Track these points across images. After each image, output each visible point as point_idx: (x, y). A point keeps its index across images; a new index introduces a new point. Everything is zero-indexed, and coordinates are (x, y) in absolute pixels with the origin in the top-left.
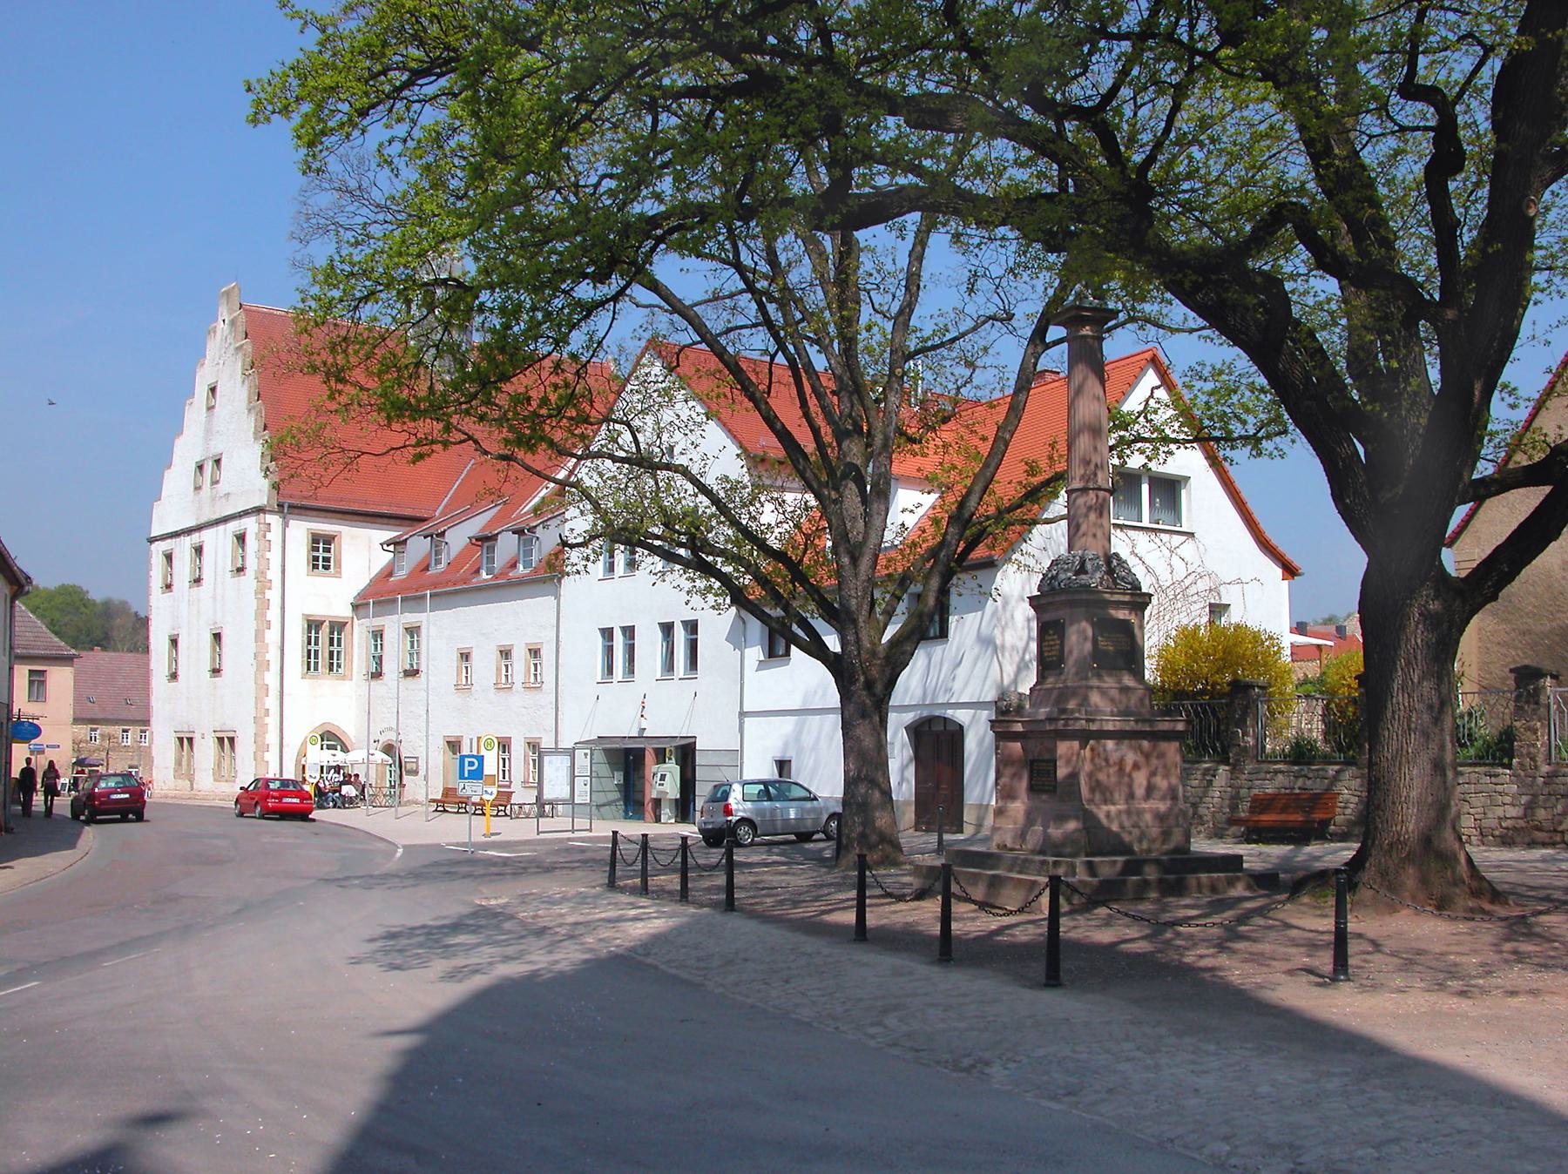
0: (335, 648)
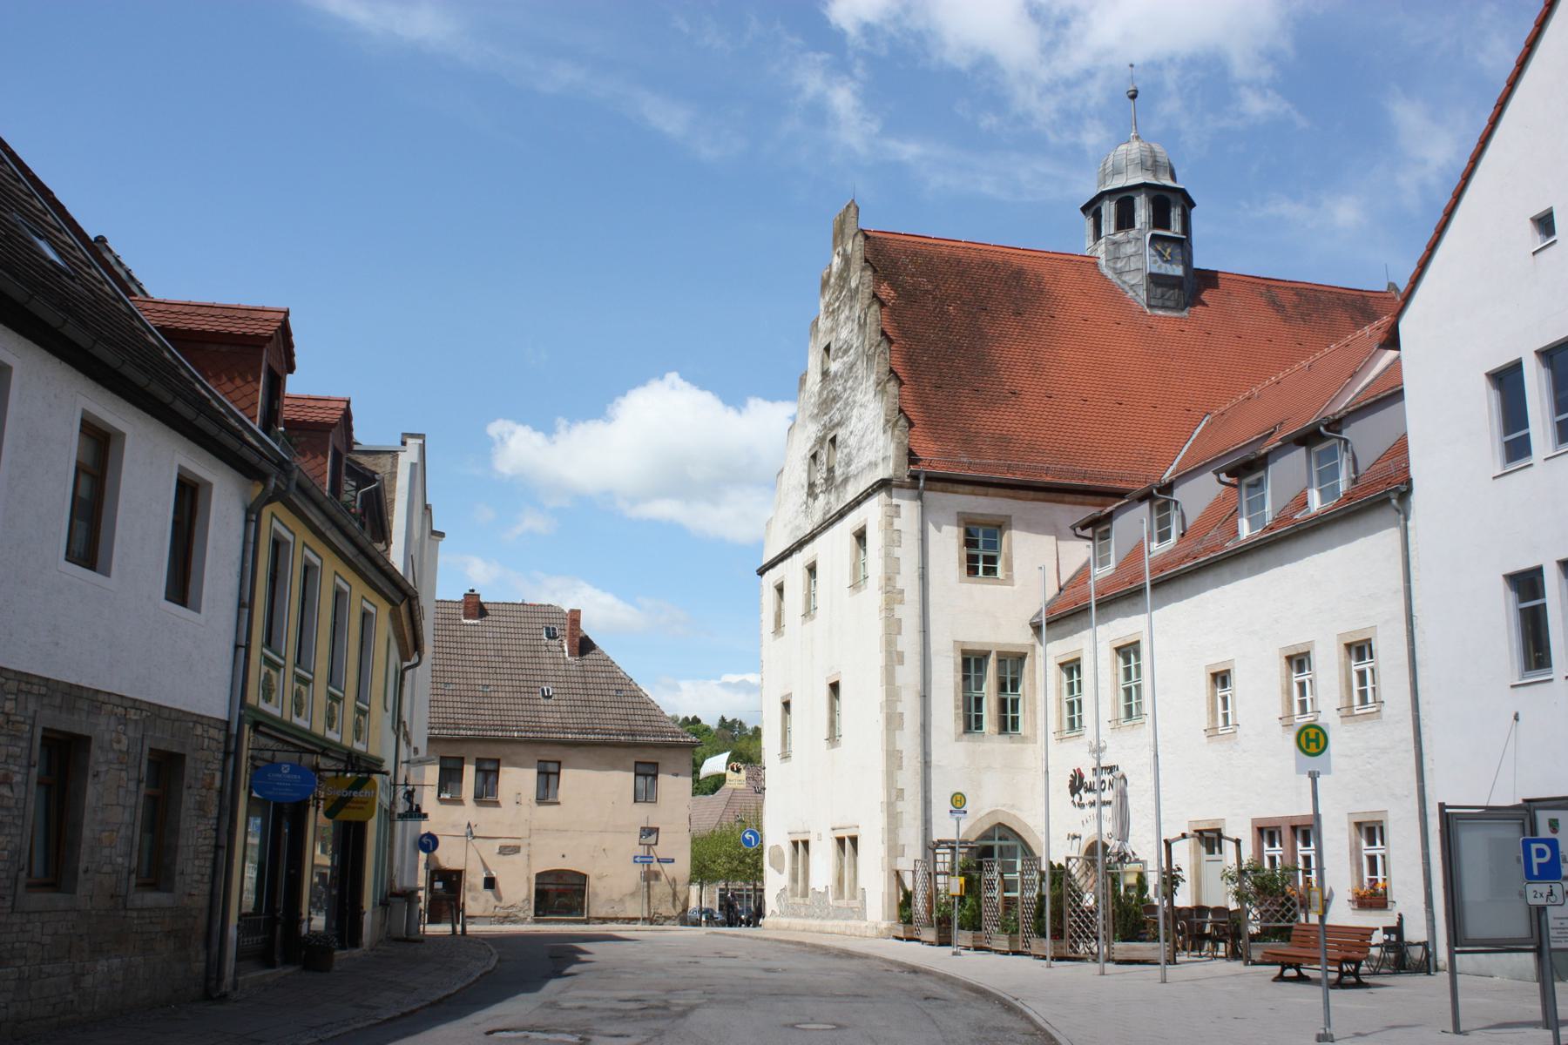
0: (1009, 695)
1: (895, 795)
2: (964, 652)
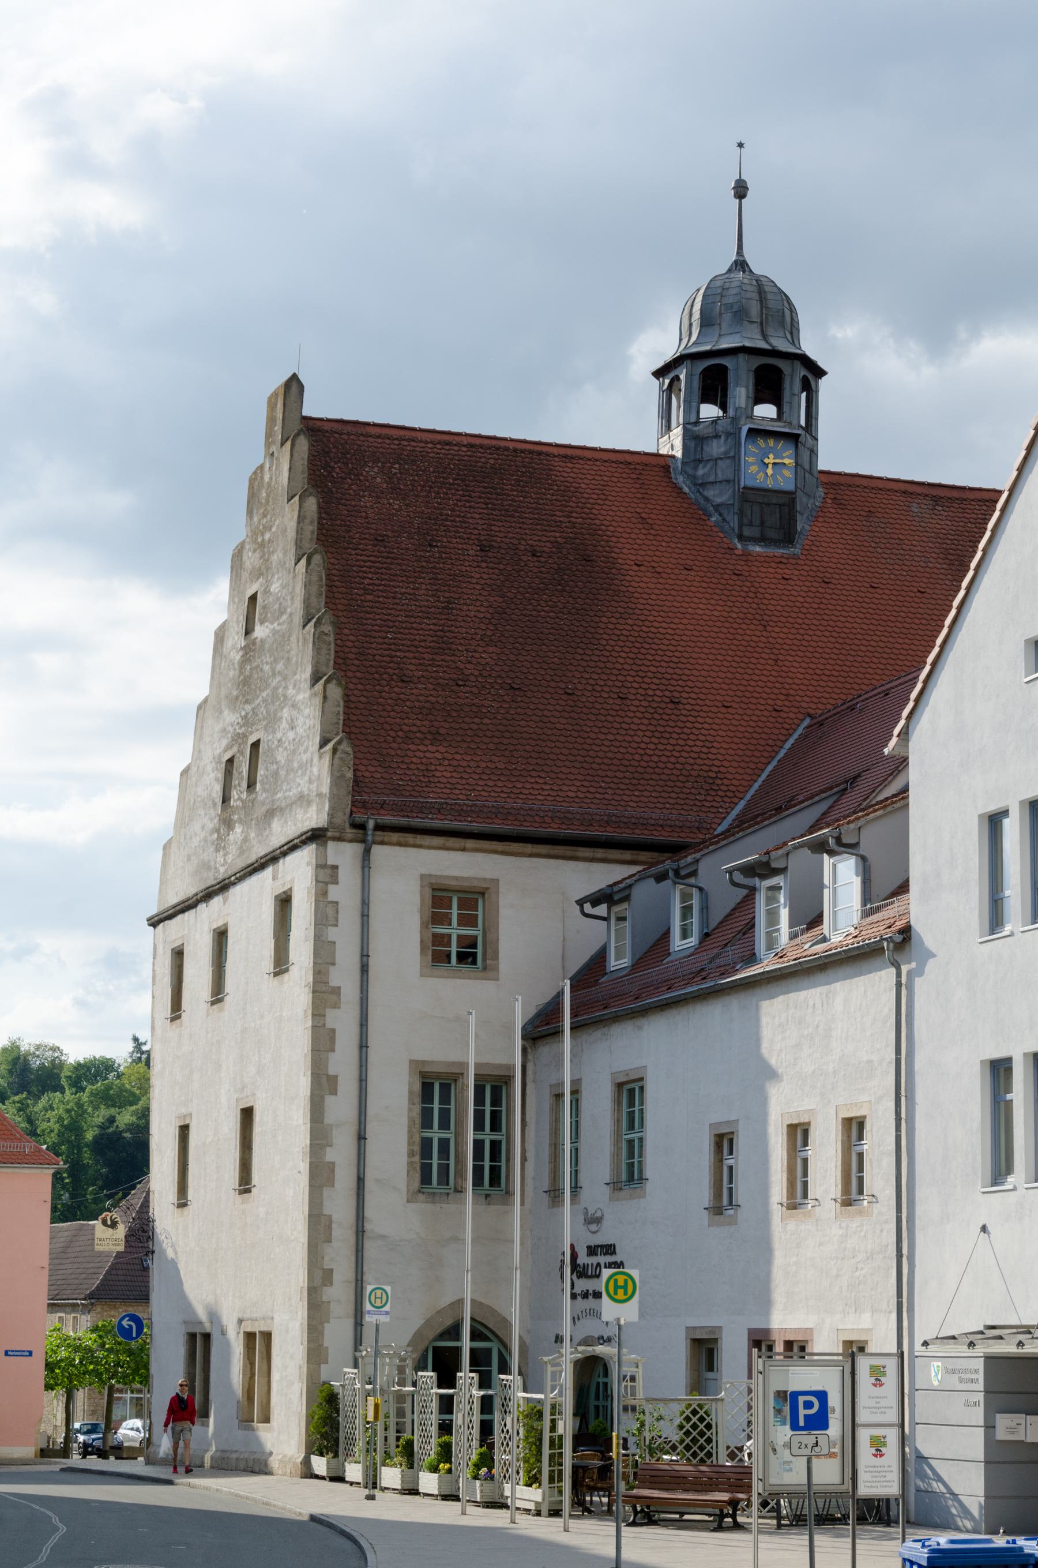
1: (319, 1277)
2: (423, 1075)
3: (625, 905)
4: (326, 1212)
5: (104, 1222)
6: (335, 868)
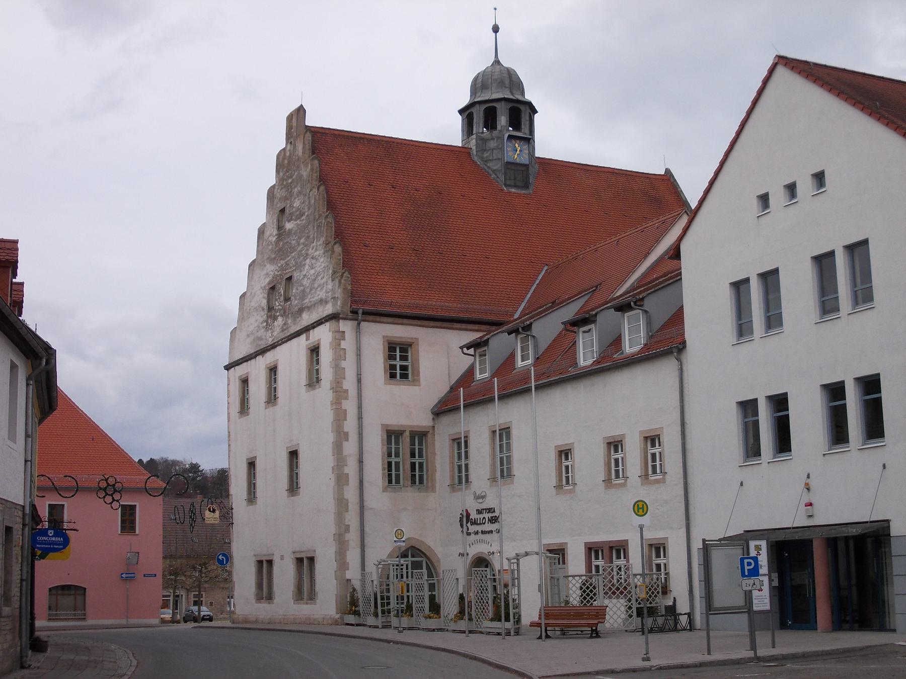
3: (485, 348)
4: (345, 497)
5: (209, 510)
6: (344, 332)
